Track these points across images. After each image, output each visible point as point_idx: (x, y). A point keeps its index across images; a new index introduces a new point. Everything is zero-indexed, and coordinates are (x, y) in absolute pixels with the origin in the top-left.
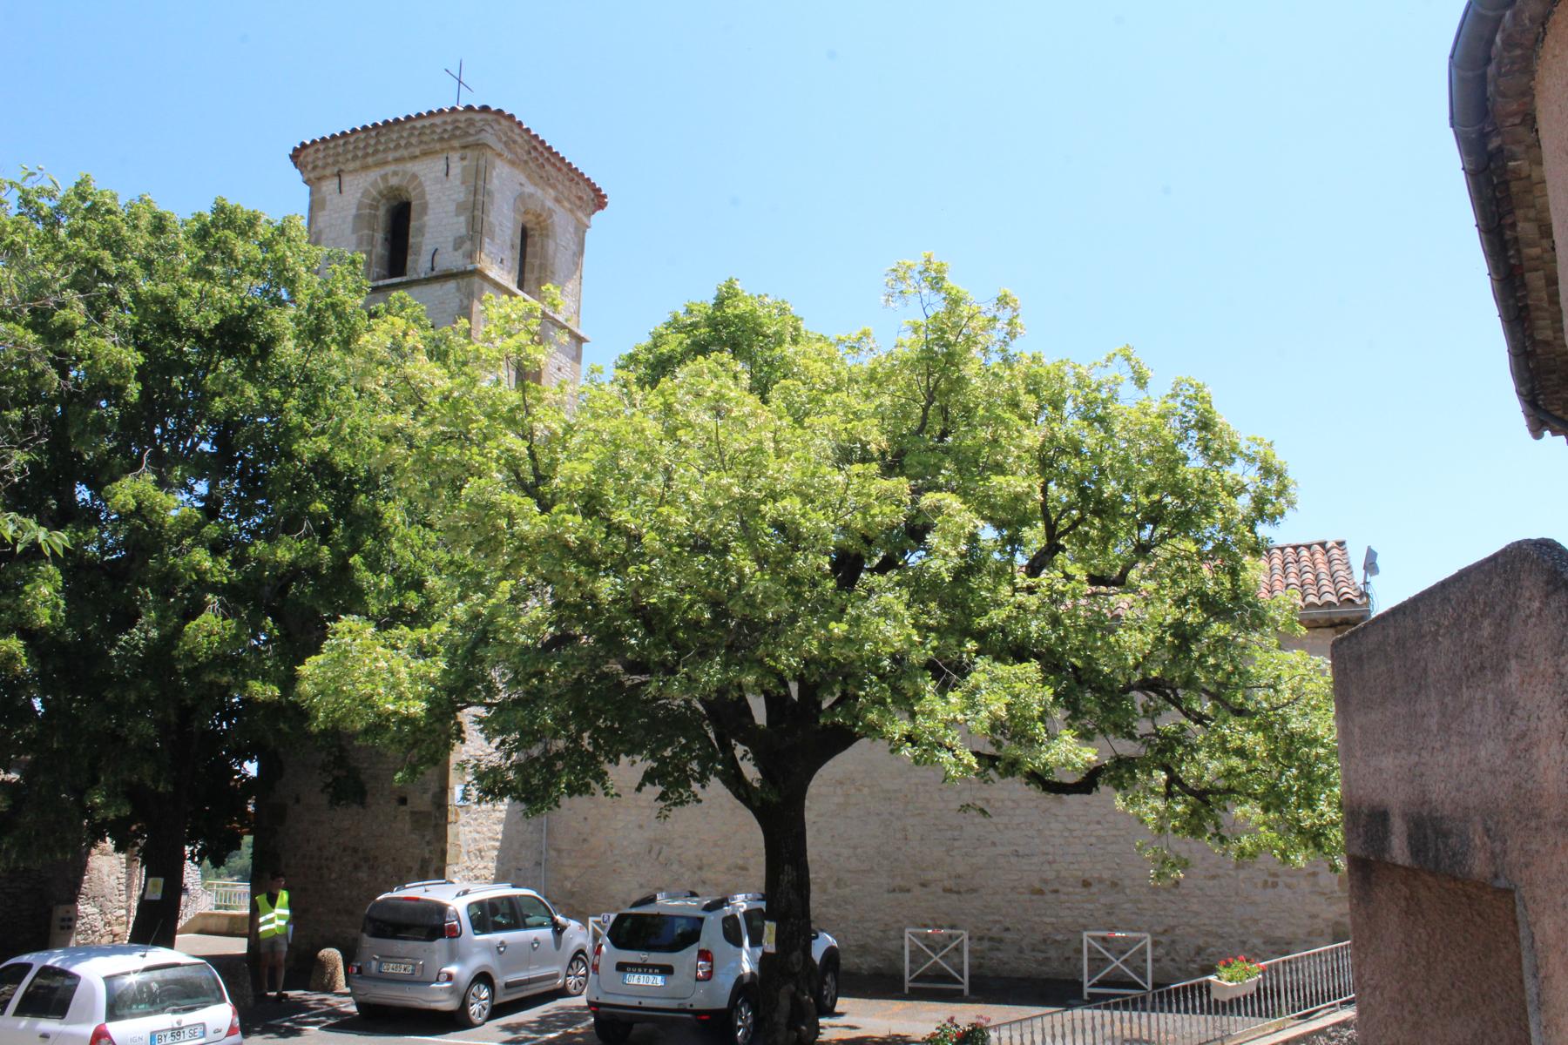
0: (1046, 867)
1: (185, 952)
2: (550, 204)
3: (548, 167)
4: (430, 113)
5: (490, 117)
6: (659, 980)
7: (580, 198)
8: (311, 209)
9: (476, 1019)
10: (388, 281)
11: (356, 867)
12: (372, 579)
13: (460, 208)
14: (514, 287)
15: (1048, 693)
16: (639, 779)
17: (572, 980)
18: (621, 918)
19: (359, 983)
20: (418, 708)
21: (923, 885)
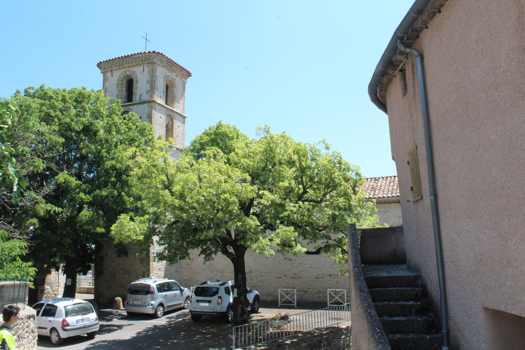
0: (319, 271)
1: (79, 299)
2: (174, 77)
3: (173, 67)
5: (155, 54)
6: (208, 304)
8: (104, 81)
9: (159, 316)
10: (127, 104)
11: (124, 274)
12: (128, 199)
13: (148, 81)
14: (164, 104)
15: (297, 234)
16: (200, 252)
17: (186, 305)
18: (197, 288)
19: (127, 307)
20: (141, 238)
21: (285, 276)
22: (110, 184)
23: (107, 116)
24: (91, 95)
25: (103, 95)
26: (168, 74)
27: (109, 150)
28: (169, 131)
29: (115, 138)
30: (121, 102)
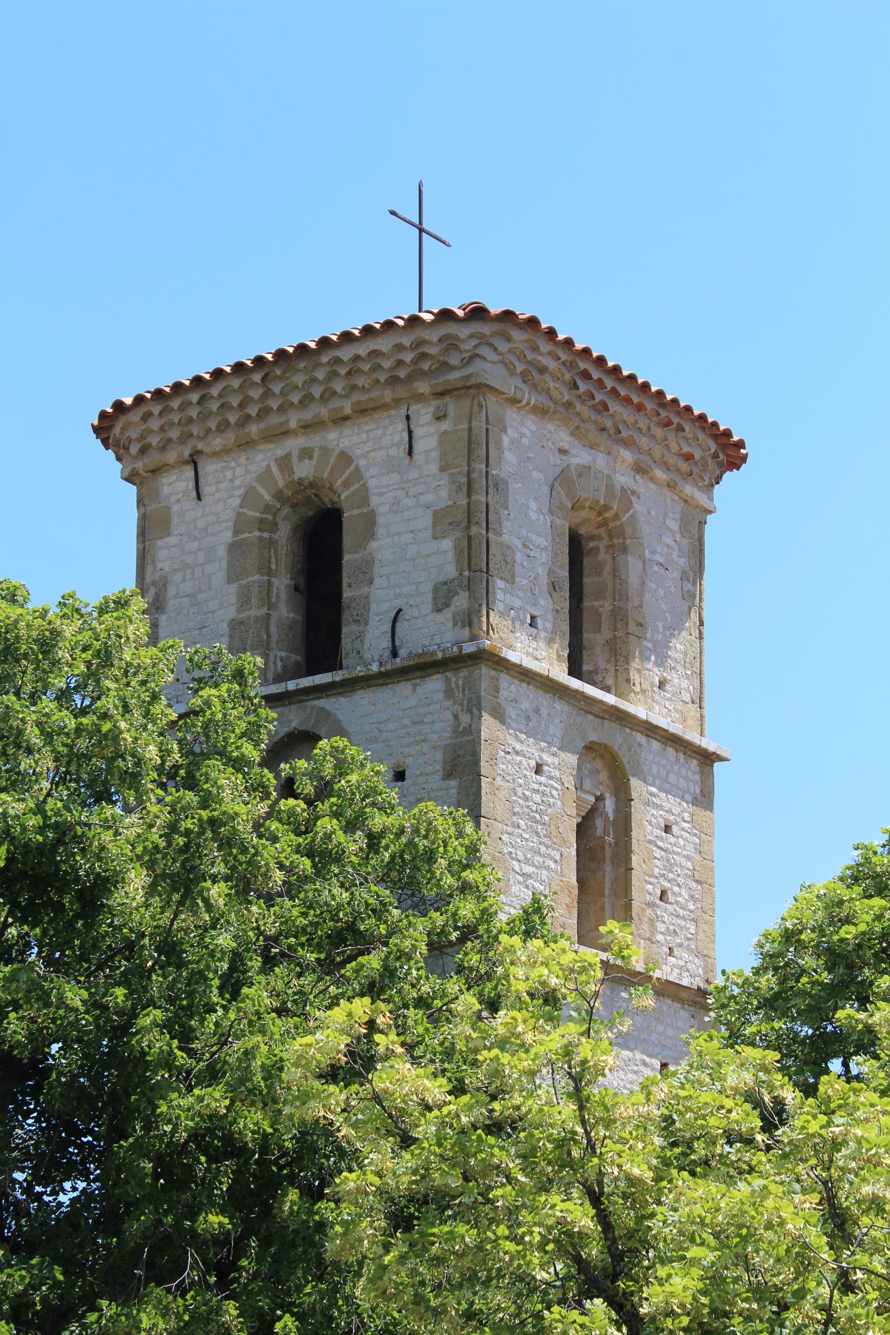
2: (624, 479)
3: (614, 407)
4: (368, 330)
5: (486, 329)
7: (688, 457)
8: (143, 534)
10: (306, 682)
13: (441, 521)
14: (560, 673)
22: (191, 1256)
23: (172, 774)
24: (56, 634)
25: (138, 628)
26: (581, 456)
27: (190, 1012)
28: (602, 856)
29: (226, 924)
30: (264, 672)
